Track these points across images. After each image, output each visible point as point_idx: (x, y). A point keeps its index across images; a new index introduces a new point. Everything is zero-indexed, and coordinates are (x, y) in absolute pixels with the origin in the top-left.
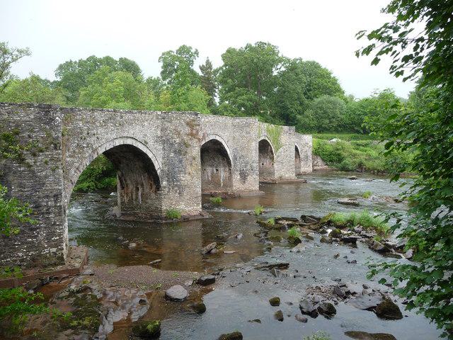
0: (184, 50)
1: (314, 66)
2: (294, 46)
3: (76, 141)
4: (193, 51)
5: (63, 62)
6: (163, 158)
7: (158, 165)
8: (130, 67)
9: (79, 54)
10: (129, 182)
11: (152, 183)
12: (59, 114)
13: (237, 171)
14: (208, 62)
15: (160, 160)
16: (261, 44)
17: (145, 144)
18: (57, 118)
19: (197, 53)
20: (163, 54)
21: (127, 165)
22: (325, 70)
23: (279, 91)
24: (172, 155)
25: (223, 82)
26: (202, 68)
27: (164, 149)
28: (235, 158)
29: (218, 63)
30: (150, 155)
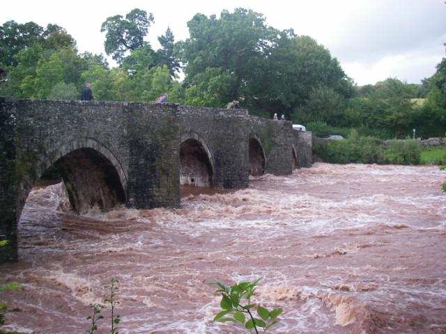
0: (136, 14)
1: (308, 38)
2: (206, 15)
3: (26, 145)
4: (148, 16)
5: (190, 18)
6: (130, 166)
7: (123, 175)
8: (59, 40)
9: (5, 22)
10: (82, 198)
11: (115, 199)
12: (14, 110)
13: (220, 181)
14: (169, 32)
15: (127, 168)
16: (240, 12)
17: (106, 145)
18: (12, 116)
19: (152, 18)
20: (109, 19)
21: (81, 174)
22: (321, 48)
23: (191, 72)
24: (142, 161)
25: (189, 57)
26: (162, 40)
27: (132, 154)
28: (218, 162)
29: (182, 35)
30: (114, 162)
